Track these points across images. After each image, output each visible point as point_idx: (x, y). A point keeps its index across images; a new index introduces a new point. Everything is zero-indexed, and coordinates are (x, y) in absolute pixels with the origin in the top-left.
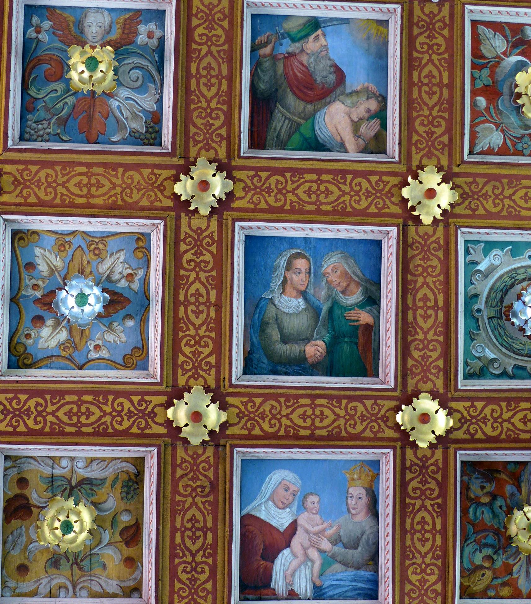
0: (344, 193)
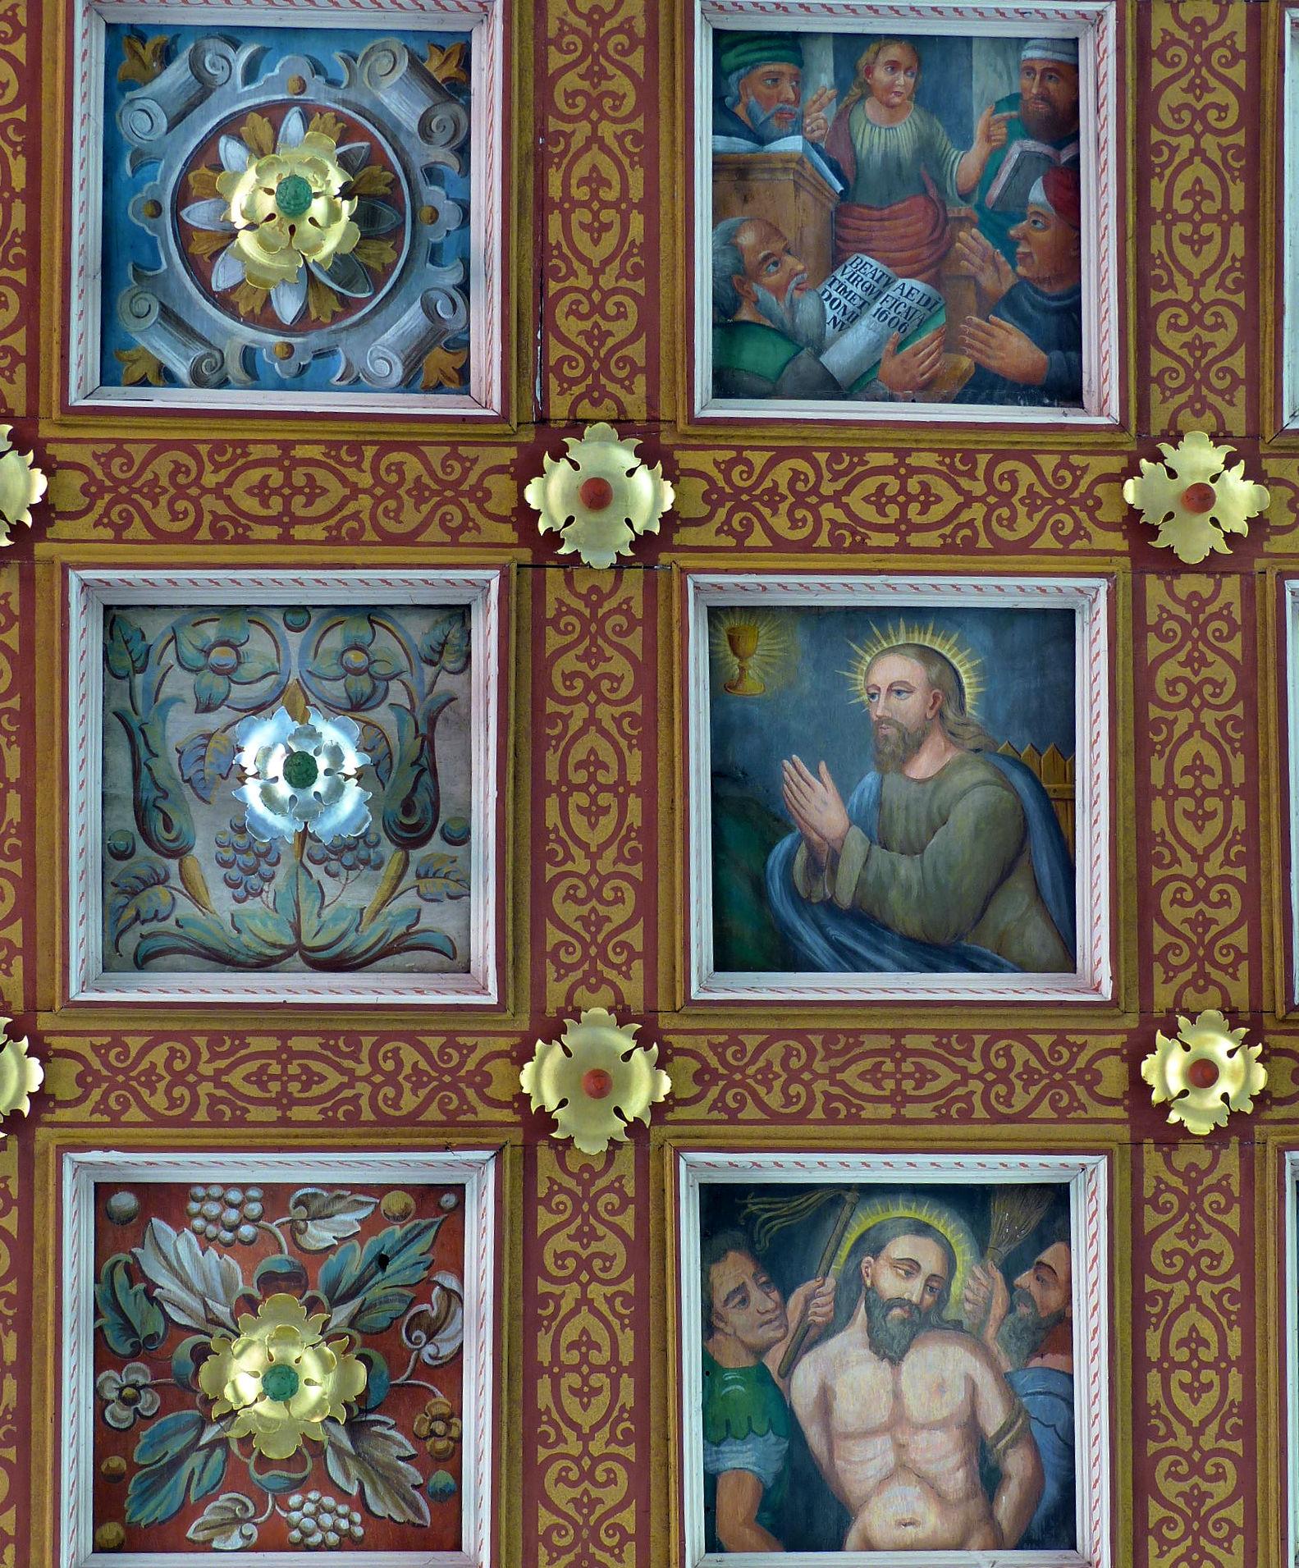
0: (596, 273)
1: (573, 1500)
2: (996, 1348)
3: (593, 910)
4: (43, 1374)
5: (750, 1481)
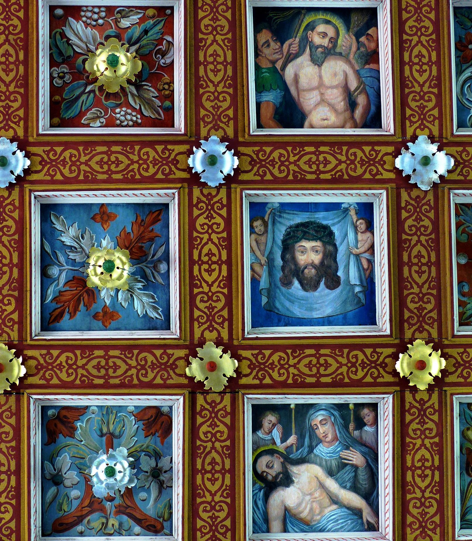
0: (216, 86)
1: (212, 106)
2: (353, 61)
3: (276, 366)
4: (33, 65)
5: (271, 105)
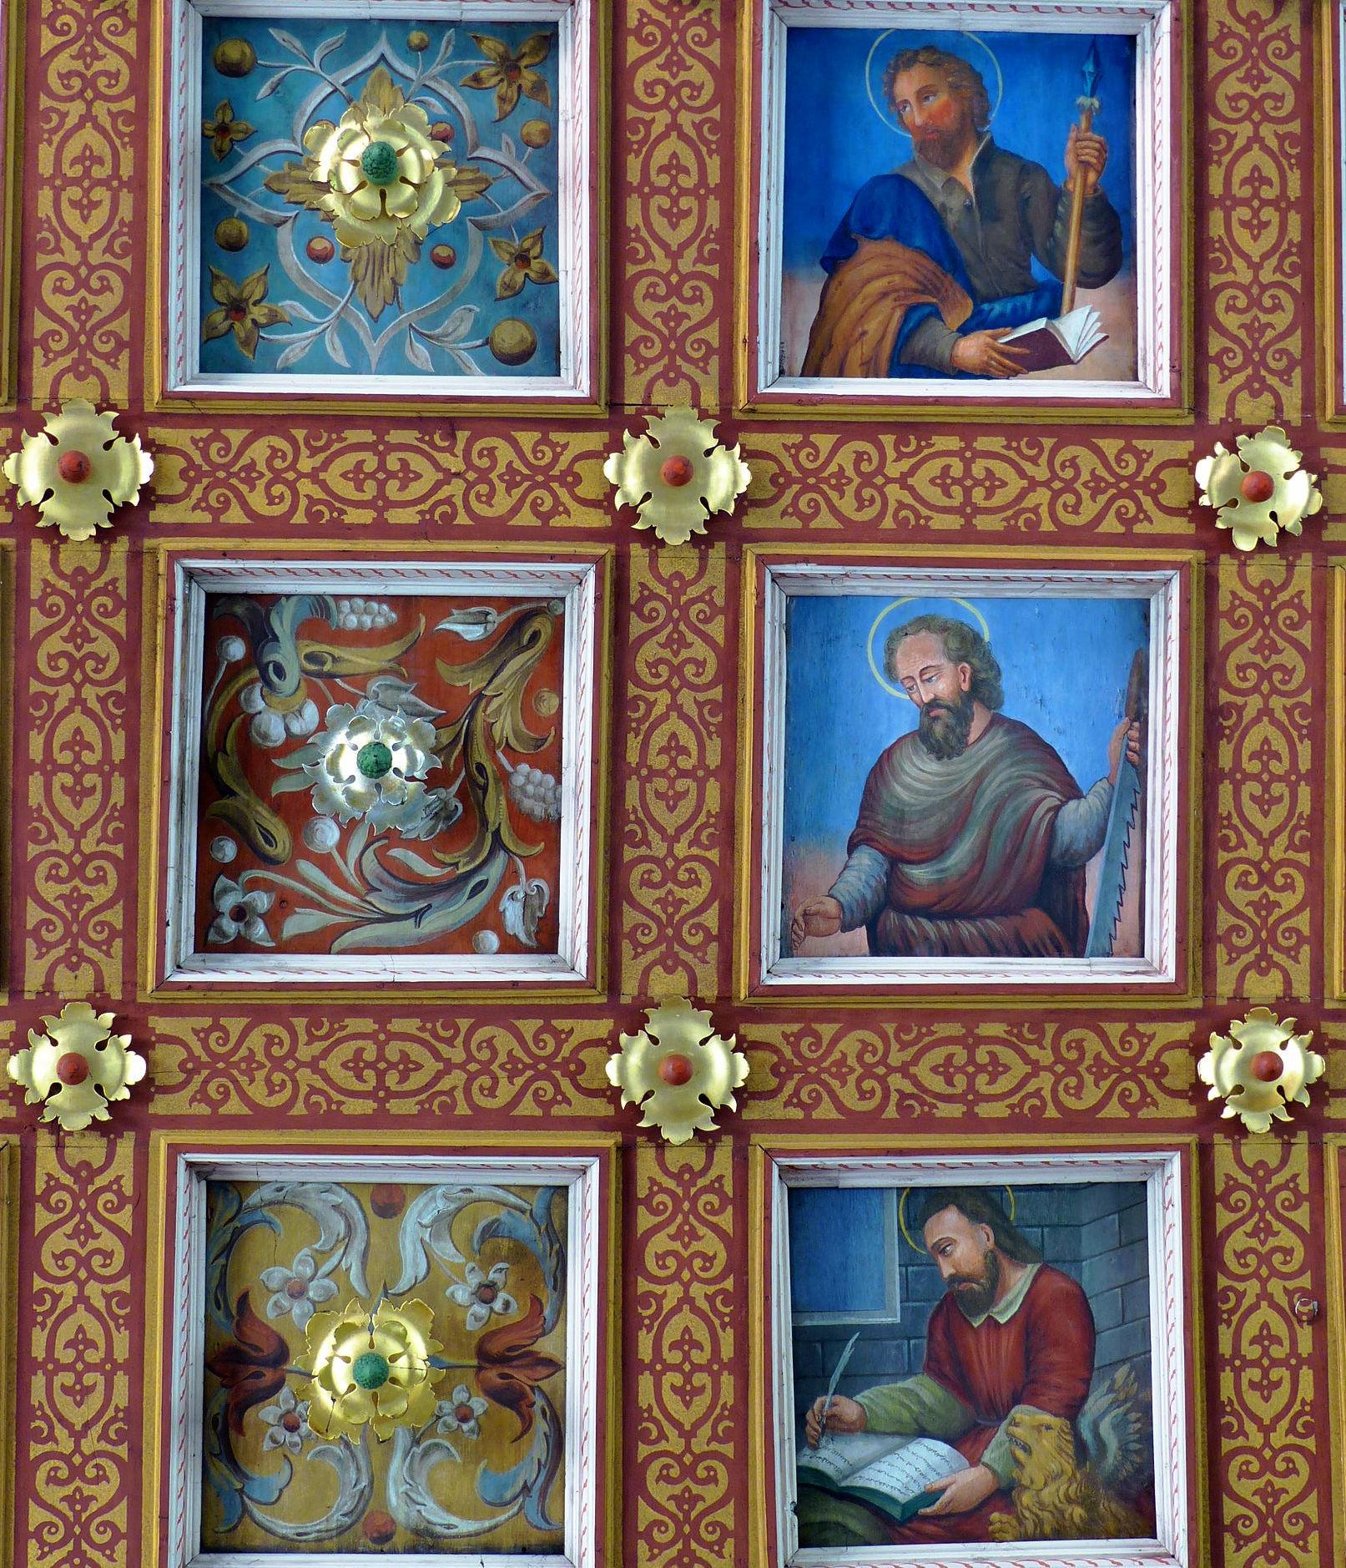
3: (852, 1070)
